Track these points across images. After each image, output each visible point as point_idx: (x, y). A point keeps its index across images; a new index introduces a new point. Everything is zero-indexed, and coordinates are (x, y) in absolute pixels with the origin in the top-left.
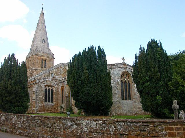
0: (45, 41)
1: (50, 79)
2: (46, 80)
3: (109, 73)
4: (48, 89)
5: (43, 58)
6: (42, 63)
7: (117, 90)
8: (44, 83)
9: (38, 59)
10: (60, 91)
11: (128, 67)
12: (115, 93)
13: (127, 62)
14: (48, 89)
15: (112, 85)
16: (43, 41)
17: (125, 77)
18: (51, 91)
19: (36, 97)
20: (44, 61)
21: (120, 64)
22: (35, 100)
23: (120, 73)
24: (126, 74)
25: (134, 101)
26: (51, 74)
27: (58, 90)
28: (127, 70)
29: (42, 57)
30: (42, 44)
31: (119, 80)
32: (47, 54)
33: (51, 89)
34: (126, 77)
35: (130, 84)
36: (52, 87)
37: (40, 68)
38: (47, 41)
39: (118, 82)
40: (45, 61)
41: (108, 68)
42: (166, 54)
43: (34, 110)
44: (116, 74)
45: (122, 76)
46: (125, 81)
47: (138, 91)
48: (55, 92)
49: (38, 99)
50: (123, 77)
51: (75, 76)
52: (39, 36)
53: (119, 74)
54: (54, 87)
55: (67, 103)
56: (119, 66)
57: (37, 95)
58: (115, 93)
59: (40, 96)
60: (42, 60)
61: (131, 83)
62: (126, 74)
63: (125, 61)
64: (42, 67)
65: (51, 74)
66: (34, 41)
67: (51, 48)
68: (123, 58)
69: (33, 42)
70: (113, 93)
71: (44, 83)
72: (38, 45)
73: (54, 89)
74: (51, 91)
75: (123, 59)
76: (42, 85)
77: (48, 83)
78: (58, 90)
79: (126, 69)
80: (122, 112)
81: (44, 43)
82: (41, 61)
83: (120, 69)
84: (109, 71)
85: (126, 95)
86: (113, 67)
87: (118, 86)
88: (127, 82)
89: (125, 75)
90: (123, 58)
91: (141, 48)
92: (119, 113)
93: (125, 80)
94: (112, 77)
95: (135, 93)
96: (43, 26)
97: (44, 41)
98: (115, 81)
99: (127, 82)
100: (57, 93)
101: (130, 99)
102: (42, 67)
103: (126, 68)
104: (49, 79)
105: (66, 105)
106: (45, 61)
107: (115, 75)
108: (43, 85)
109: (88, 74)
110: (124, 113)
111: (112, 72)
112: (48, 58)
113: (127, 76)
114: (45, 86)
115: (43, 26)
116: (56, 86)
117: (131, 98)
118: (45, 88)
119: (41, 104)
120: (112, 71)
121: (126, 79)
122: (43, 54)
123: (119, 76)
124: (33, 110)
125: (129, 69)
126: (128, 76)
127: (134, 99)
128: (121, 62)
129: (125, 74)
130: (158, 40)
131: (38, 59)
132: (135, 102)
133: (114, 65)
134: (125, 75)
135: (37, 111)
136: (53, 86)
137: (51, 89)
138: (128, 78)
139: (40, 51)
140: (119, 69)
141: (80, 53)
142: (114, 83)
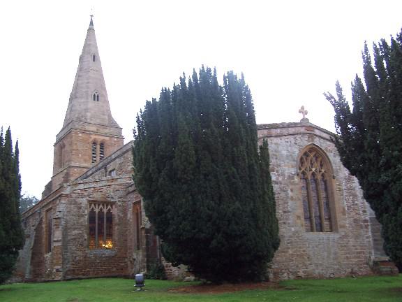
0: (99, 97)
1: (104, 183)
2: (93, 185)
3: (265, 148)
4: (97, 210)
5: (95, 139)
6: (94, 150)
7: (290, 203)
8: (86, 194)
10: (130, 216)
11: (317, 132)
12: (285, 212)
13: (314, 120)
14: (97, 210)
15: (276, 188)
16: (94, 95)
17: (312, 164)
18: (105, 217)
19: (65, 235)
20: (98, 147)
21: (294, 125)
22: (60, 244)
23: (296, 152)
24: (314, 153)
25: (343, 234)
26: (111, 172)
27: (125, 214)
28: (317, 142)
29: (93, 137)
31: (293, 171)
32: (105, 127)
33: (105, 211)
34: (316, 164)
35: (328, 182)
36: (109, 207)
38: (105, 96)
39: (291, 177)
40: (102, 145)
41: (260, 134)
43: (57, 270)
44: (284, 153)
45: (301, 159)
46: (313, 174)
47: (367, 197)
48: (116, 220)
49: (69, 238)
50: (307, 164)
51: (151, 160)
53: (294, 153)
54: (114, 206)
55: (147, 250)
56: (291, 130)
57: (66, 229)
58: (285, 212)
59: (76, 232)
60: (94, 143)
61: (331, 182)
62: (314, 153)
63: (306, 116)
65: (111, 172)
66: (73, 97)
67: (114, 116)
68: (303, 108)
69: (71, 99)
70: (279, 212)
71: (86, 194)
73: (115, 211)
74: (105, 217)
75: (303, 111)
76: (80, 200)
77: (98, 196)
78: (125, 211)
79: (313, 140)
80: (310, 268)
83: (295, 139)
84: (266, 144)
85: (321, 217)
86: (274, 132)
87: (292, 190)
88: (319, 177)
89: (312, 155)
90: (303, 108)
91: (366, 50)
92: (301, 274)
93: (311, 172)
94: (273, 161)
95: (344, 209)
96: (94, 56)
97: (98, 97)
98: (283, 175)
99: (319, 177)
100: (123, 220)
101: (331, 230)
103: (312, 136)
104: (100, 184)
105: (145, 253)
106: (102, 145)
107: (282, 155)
108: (84, 201)
109: (196, 151)
110: (317, 271)
111: (271, 148)
112: (107, 138)
113: (316, 160)
114: (90, 203)
115: (94, 56)
116: (119, 204)
117: (334, 228)
118: (90, 210)
119: (79, 253)
120: (273, 145)
121: (313, 169)
122: (93, 128)
123: (294, 161)
124: (54, 271)
125: (322, 141)
126: (319, 159)
127: (343, 227)
128: (297, 118)
129: (312, 155)
132: (346, 236)
133: (275, 126)
134: (312, 155)
135: (66, 274)
136: (112, 204)
137: (105, 211)
138: (321, 165)
139: (89, 121)
140: (292, 138)
142: (280, 179)
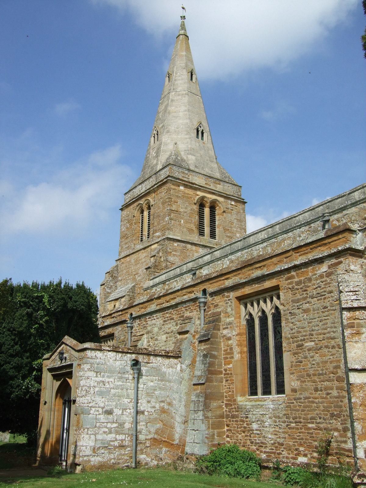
4: (255, 311)
9: (185, 197)
14: (255, 311)
20: (207, 211)
30: (195, 144)
37: (195, 238)
42: (24, 444)
52: (181, 114)
64: (202, 233)
68: (181, 17)
72: (182, 147)
81: (202, 139)
82: (196, 208)
90: (181, 17)
97: (202, 133)
102: (202, 233)
115: (101, 285)
130: (87, 285)
131: (185, 197)
139: (192, 168)
141: (60, 283)
